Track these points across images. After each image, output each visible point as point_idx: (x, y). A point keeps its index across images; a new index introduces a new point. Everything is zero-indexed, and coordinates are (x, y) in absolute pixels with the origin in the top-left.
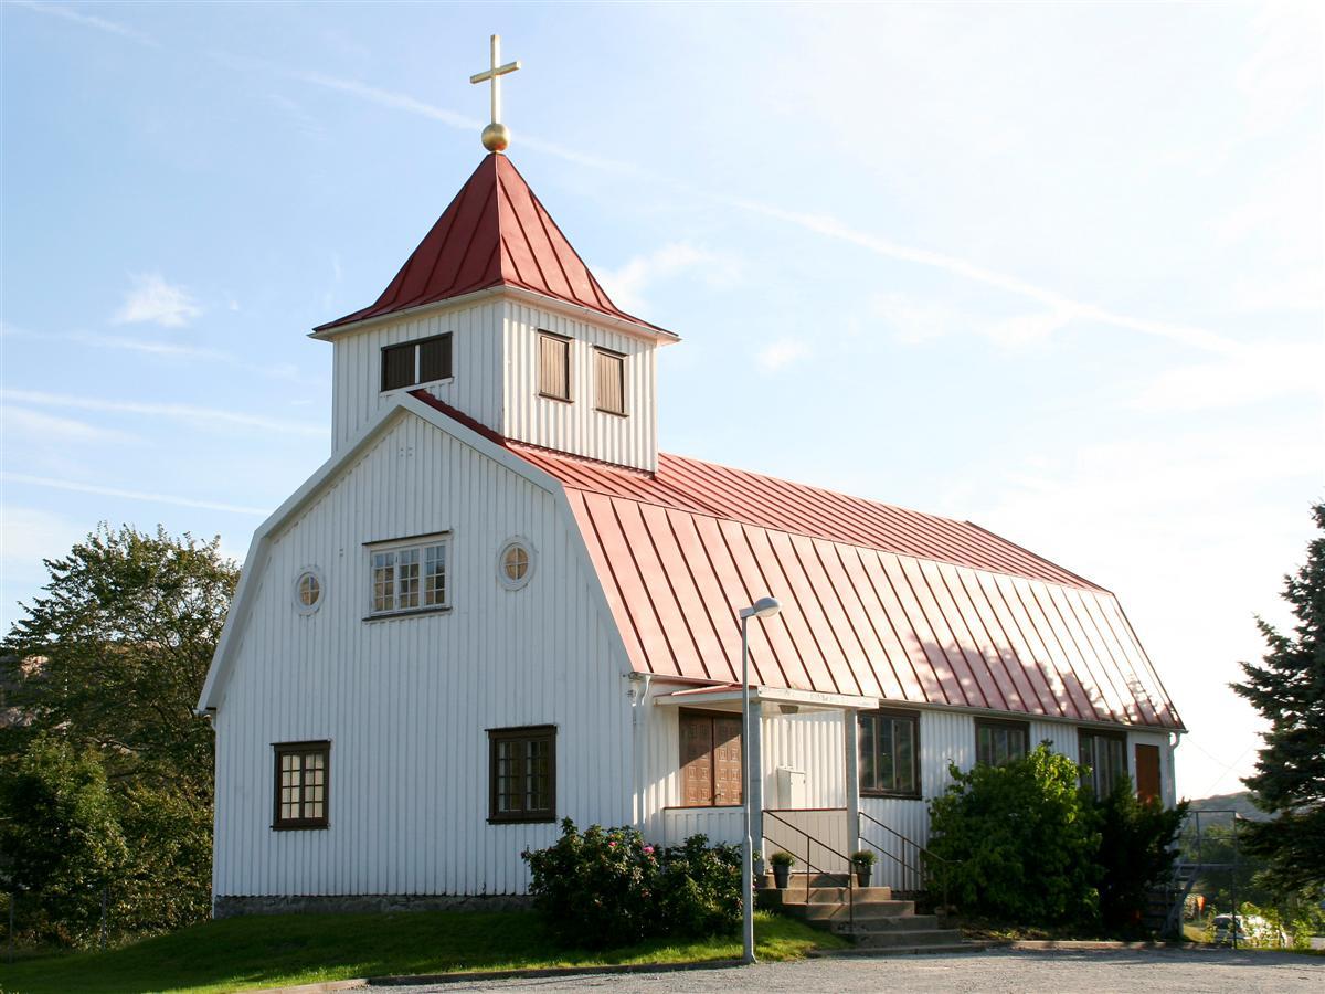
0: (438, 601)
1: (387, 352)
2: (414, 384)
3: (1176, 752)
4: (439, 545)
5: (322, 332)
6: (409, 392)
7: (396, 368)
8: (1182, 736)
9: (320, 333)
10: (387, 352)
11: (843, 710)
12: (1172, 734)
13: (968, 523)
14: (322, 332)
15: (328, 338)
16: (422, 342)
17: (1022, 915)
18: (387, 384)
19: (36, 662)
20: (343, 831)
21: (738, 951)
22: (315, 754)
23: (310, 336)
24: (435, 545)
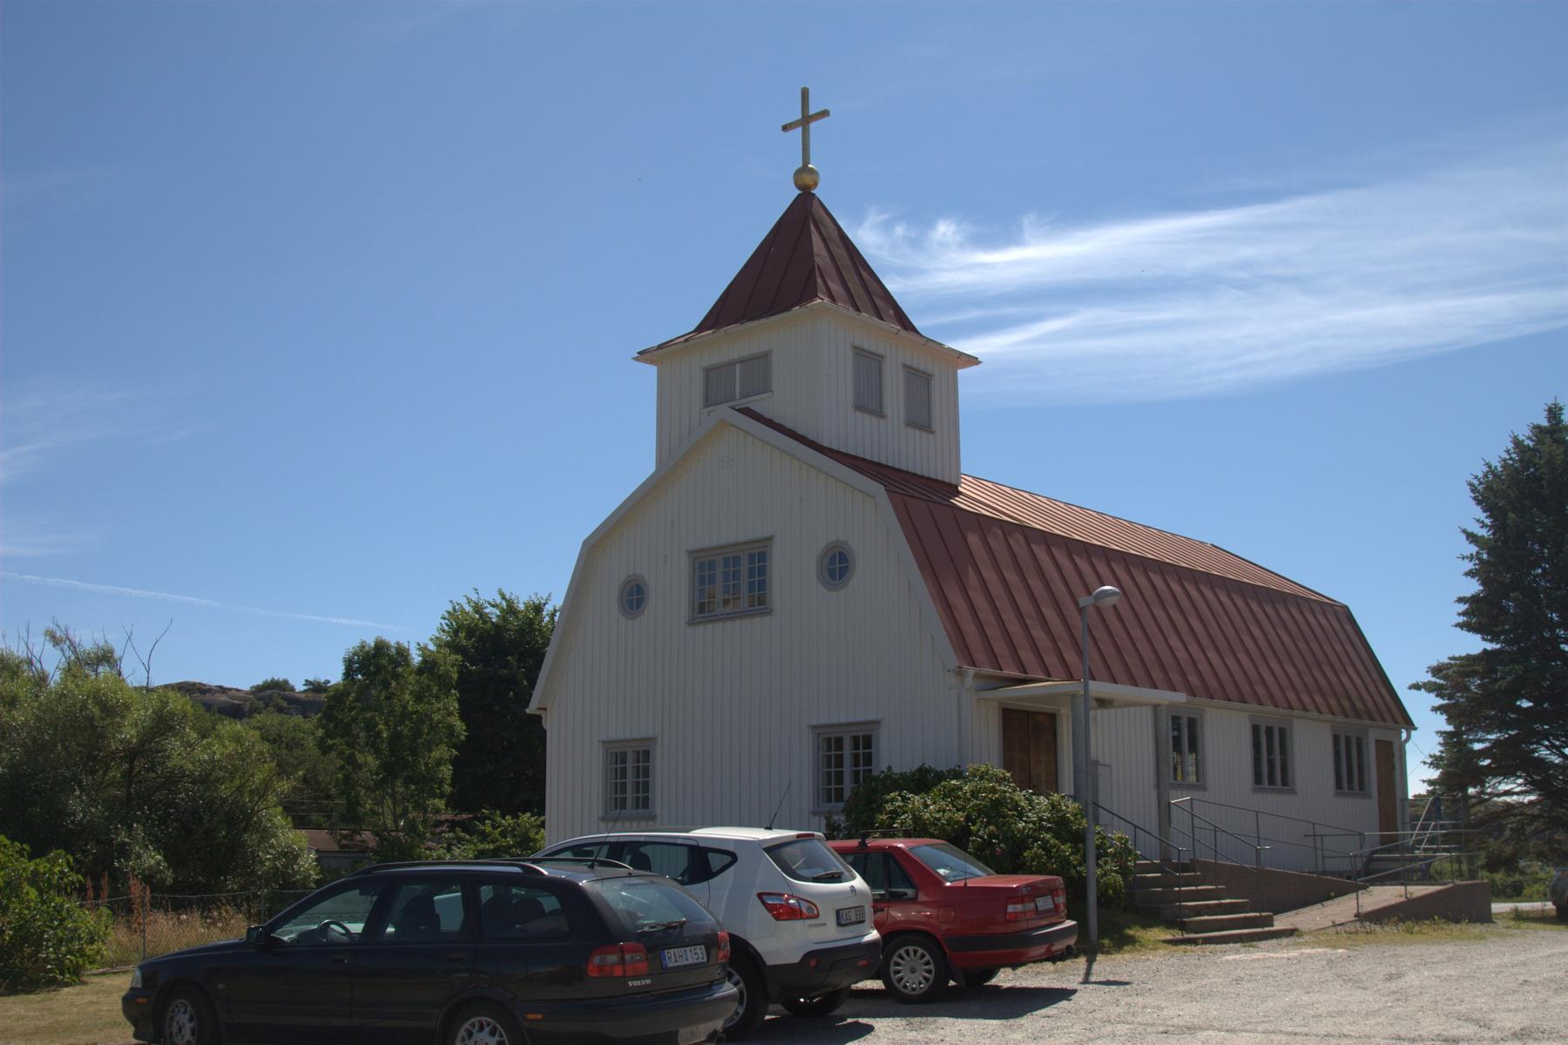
0: (760, 603)
1: (708, 371)
2: (735, 400)
3: (1408, 746)
4: (761, 550)
5: (644, 355)
6: (730, 407)
7: (716, 385)
8: (1413, 732)
9: (644, 356)
10: (708, 371)
11: (686, 849)
12: (1403, 730)
13: (1212, 545)
14: (644, 355)
15: (651, 362)
16: (743, 361)
17: (155, 730)
18: (708, 402)
19: (1389, 988)
20: (997, 612)
21: (619, 762)
22: (1356, 891)
23: (636, 359)
24: (757, 607)
